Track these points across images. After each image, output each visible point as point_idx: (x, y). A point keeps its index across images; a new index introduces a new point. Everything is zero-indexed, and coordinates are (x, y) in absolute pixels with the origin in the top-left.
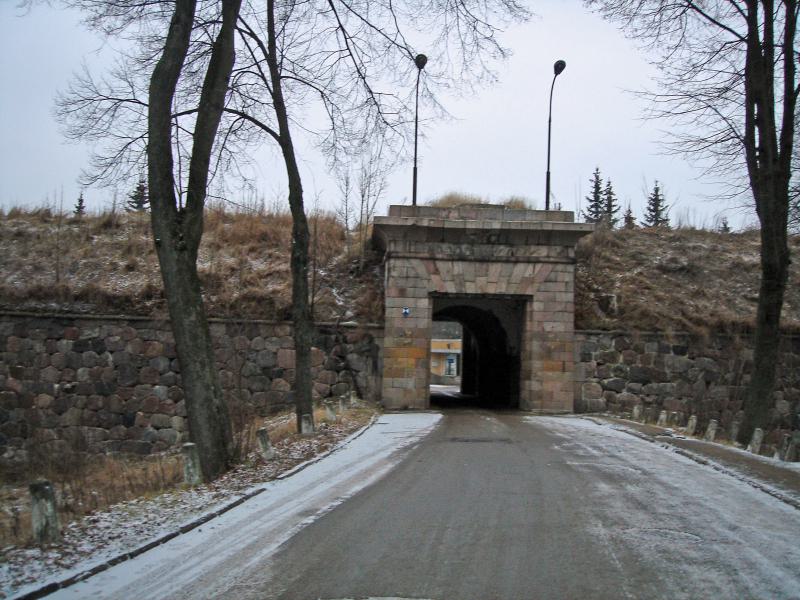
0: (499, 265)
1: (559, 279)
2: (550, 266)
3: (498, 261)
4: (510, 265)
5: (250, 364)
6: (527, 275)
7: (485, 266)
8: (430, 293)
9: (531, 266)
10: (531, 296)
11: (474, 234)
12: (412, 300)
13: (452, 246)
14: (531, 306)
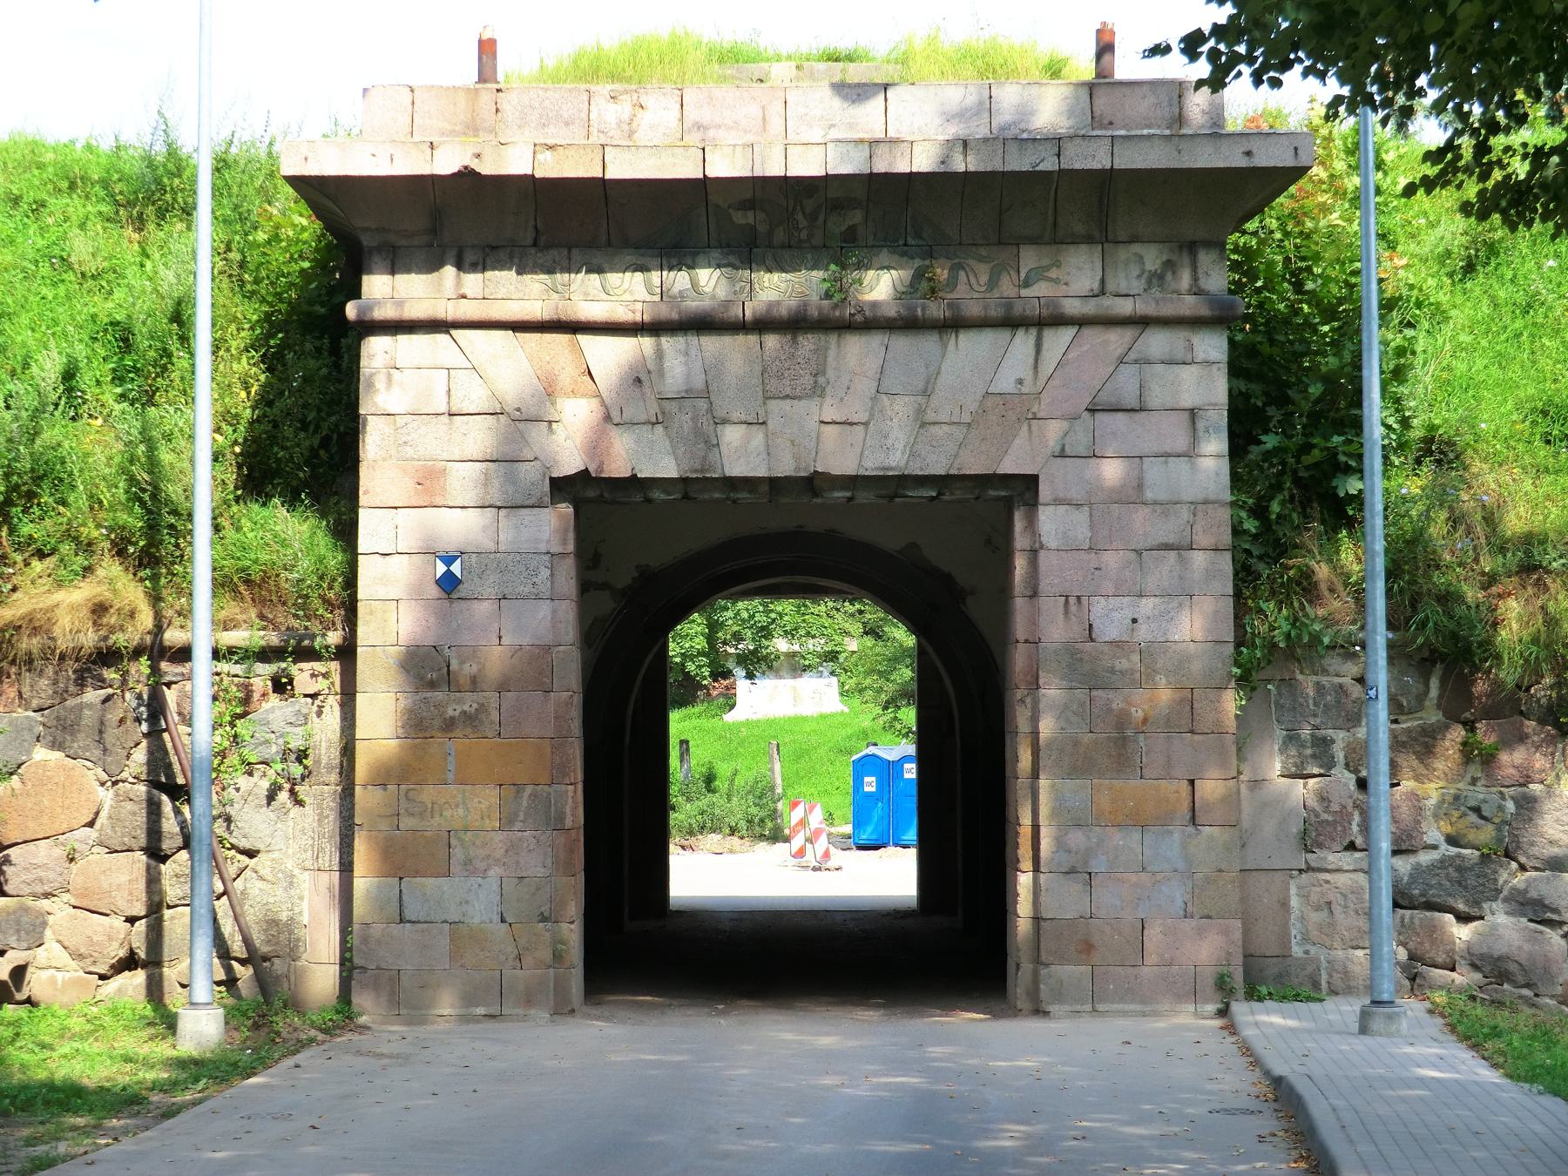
0: (876, 341)
1: (1156, 397)
2: (1116, 339)
4: (928, 343)
5: (461, 811)
6: (1005, 383)
7: (808, 342)
9: (1023, 342)
10: (1031, 482)
11: (749, 205)
14: (1031, 522)
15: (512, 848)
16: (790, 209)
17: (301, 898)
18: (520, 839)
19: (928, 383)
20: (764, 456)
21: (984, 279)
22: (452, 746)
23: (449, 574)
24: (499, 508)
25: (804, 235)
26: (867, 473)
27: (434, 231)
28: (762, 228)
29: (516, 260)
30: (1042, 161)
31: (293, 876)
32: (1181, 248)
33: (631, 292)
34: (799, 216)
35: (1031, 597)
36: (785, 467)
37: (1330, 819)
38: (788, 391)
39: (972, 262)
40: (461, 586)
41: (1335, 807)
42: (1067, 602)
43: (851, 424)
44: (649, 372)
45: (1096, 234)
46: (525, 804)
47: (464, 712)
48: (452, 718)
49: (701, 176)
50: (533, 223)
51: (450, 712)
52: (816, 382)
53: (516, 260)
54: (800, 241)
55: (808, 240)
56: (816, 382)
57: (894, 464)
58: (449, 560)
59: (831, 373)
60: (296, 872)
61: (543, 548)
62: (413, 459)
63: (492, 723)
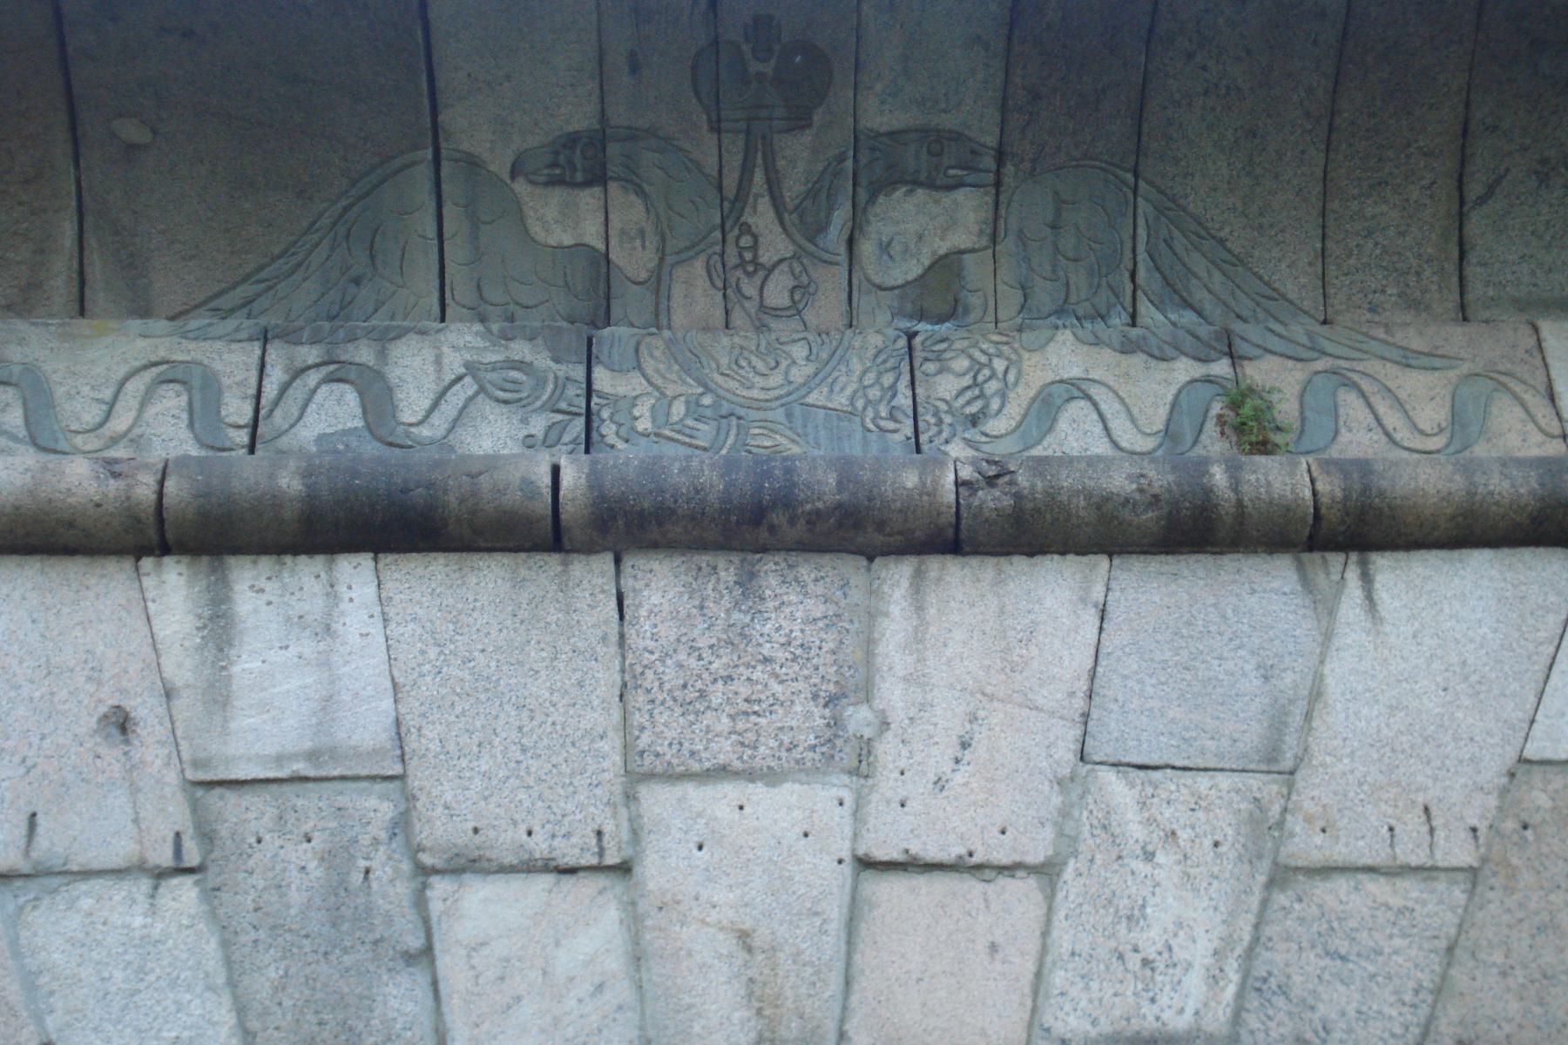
16: (731, 182)
20: (621, 991)
34: (762, 217)
38: (724, 750)
56: (836, 723)
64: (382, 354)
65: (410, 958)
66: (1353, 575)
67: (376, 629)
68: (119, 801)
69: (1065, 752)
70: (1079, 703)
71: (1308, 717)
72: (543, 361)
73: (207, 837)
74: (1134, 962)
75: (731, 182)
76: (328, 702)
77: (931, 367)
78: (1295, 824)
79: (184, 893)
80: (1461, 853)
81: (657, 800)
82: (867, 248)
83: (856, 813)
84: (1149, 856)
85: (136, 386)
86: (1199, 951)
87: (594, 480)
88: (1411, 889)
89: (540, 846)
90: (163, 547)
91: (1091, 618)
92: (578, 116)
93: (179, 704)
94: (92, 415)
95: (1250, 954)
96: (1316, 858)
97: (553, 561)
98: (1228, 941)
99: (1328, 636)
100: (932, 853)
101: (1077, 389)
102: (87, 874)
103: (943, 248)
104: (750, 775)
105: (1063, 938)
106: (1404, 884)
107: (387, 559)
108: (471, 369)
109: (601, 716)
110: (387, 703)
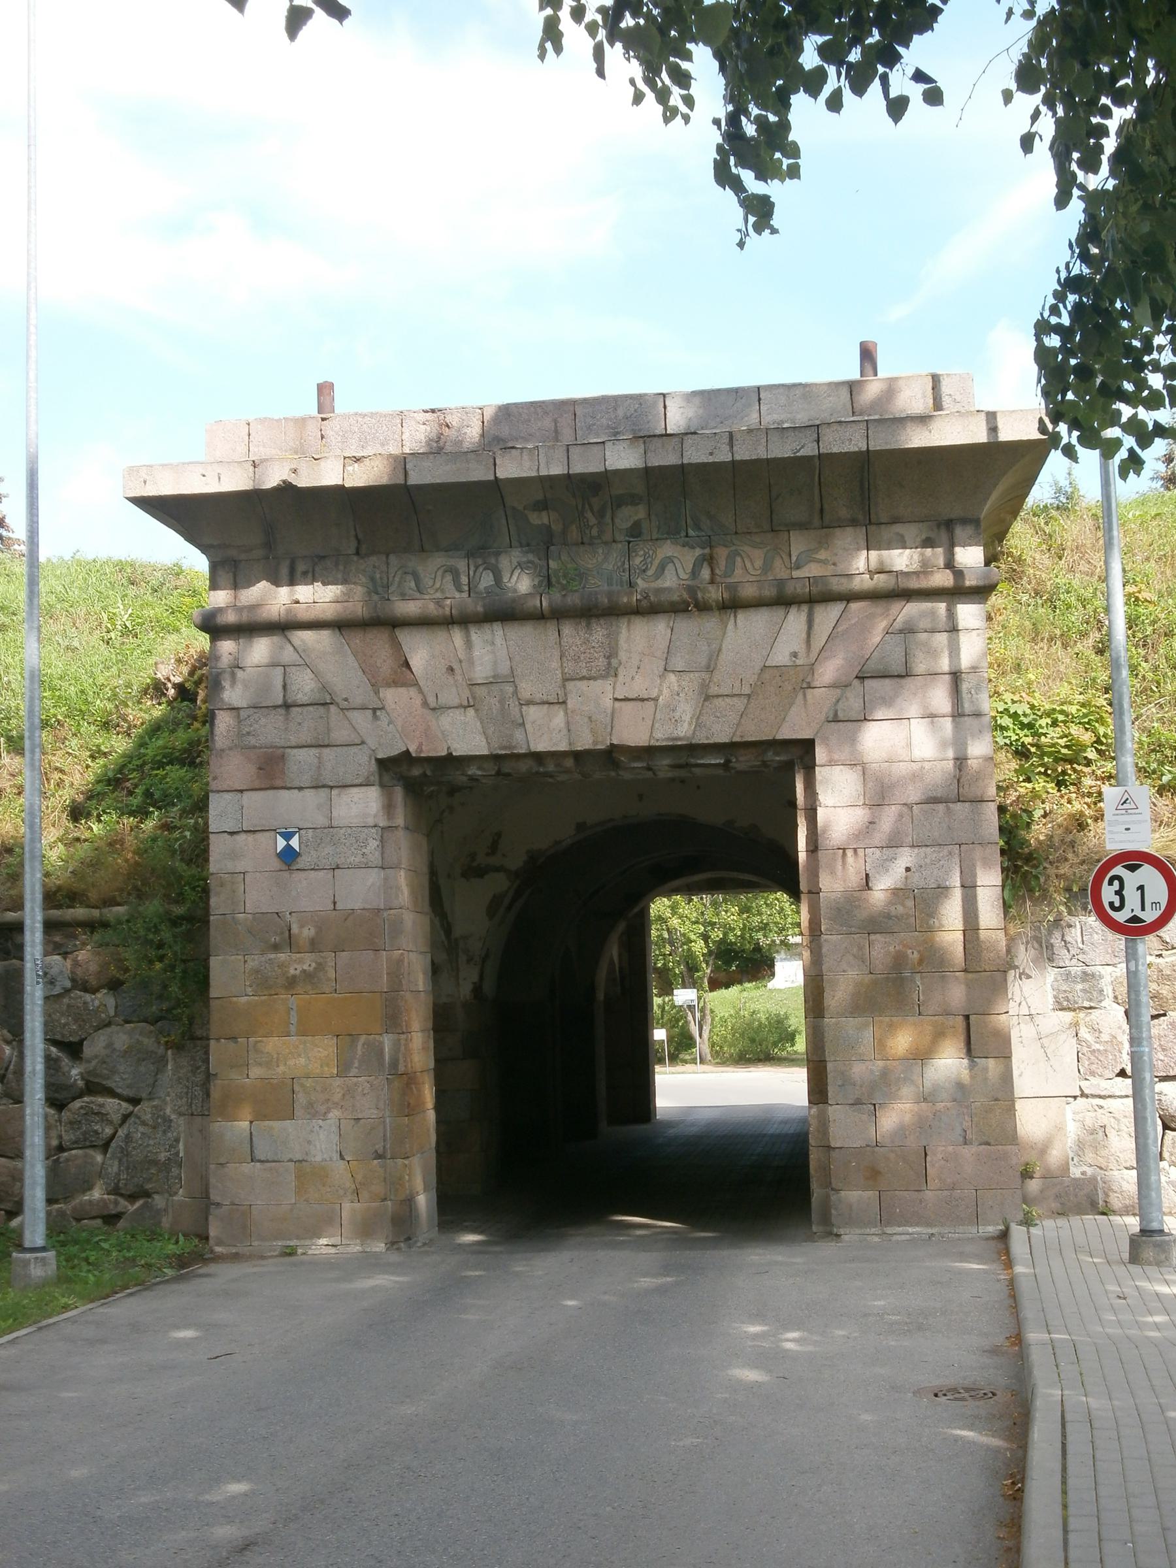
3: (650, 609)
4: (710, 623)
7: (599, 632)
8: (383, 764)
11: (542, 506)
12: (311, 798)
13: (461, 565)
15: (349, 1092)
16: (580, 507)
17: (177, 1140)
18: (356, 1085)
19: (710, 660)
20: (565, 732)
21: (759, 563)
22: (293, 1001)
23: (289, 847)
24: (332, 787)
25: (595, 532)
26: (658, 744)
27: (269, 545)
28: (557, 528)
29: (341, 567)
30: (803, 447)
31: (171, 1121)
32: (939, 526)
33: (443, 591)
34: (589, 515)
35: (813, 851)
36: (585, 742)
37: (1102, 1048)
38: (584, 673)
39: (746, 548)
40: (299, 860)
41: (1105, 1037)
42: (844, 854)
43: (643, 700)
44: (461, 661)
45: (861, 517)
46: (359, 1052)
47: (304, 971)
48: (294, 977)
49: (492, 478)
50: (353, 533)
51: (292, 972)
52: (609, 664)
53: (341, 567)
54: (592, 537)
55: (599, 537)
56: (609, 664)
57: (682, 735)
58: (288, 836)
59: (623, 655)
60: (173, 1117)
61: (371, 821)
62: (255, 747)
63: (329, 980)
64: (497, 560)
65: (520, 725)
66: (732, 615)
67: (504, 643)
68: (454, 689)
69: (661, 669)
70: (665, 655)
71: (718, 656)
72: (536, 561)
73: (474, 698)
74: (673, 720)
75: (580, 507)
76: (495, 663)
77: (634, 554)
78: (711, 685)
79: (471, 712)
80: (746, 690)
81: (570, 685)
82: (617, 521)
83: (614, 687)
84: (678, 694)
85: (440, 573)
86: (687, 718)
87: (550, 605)
88: (735, 699)
89: (545, 698)
90: (453, 623)
91: (669, 631)
92: (540, 497)
93: (463, 664)
94: (430, 583)
95: (698, 718)
96: (716, 693)
97: (543, 621)
98: (694, 715)
99: (724, 633)
100: (630, 697)
101: (670, 560)
102: (450, 708)
103: (636, 518)
104: (589, 679)
105: (658, 716)
106: (734, 699)
107: (504, 623)
108: (519, 564)
109: (555, 664)
110: (508, 663)
